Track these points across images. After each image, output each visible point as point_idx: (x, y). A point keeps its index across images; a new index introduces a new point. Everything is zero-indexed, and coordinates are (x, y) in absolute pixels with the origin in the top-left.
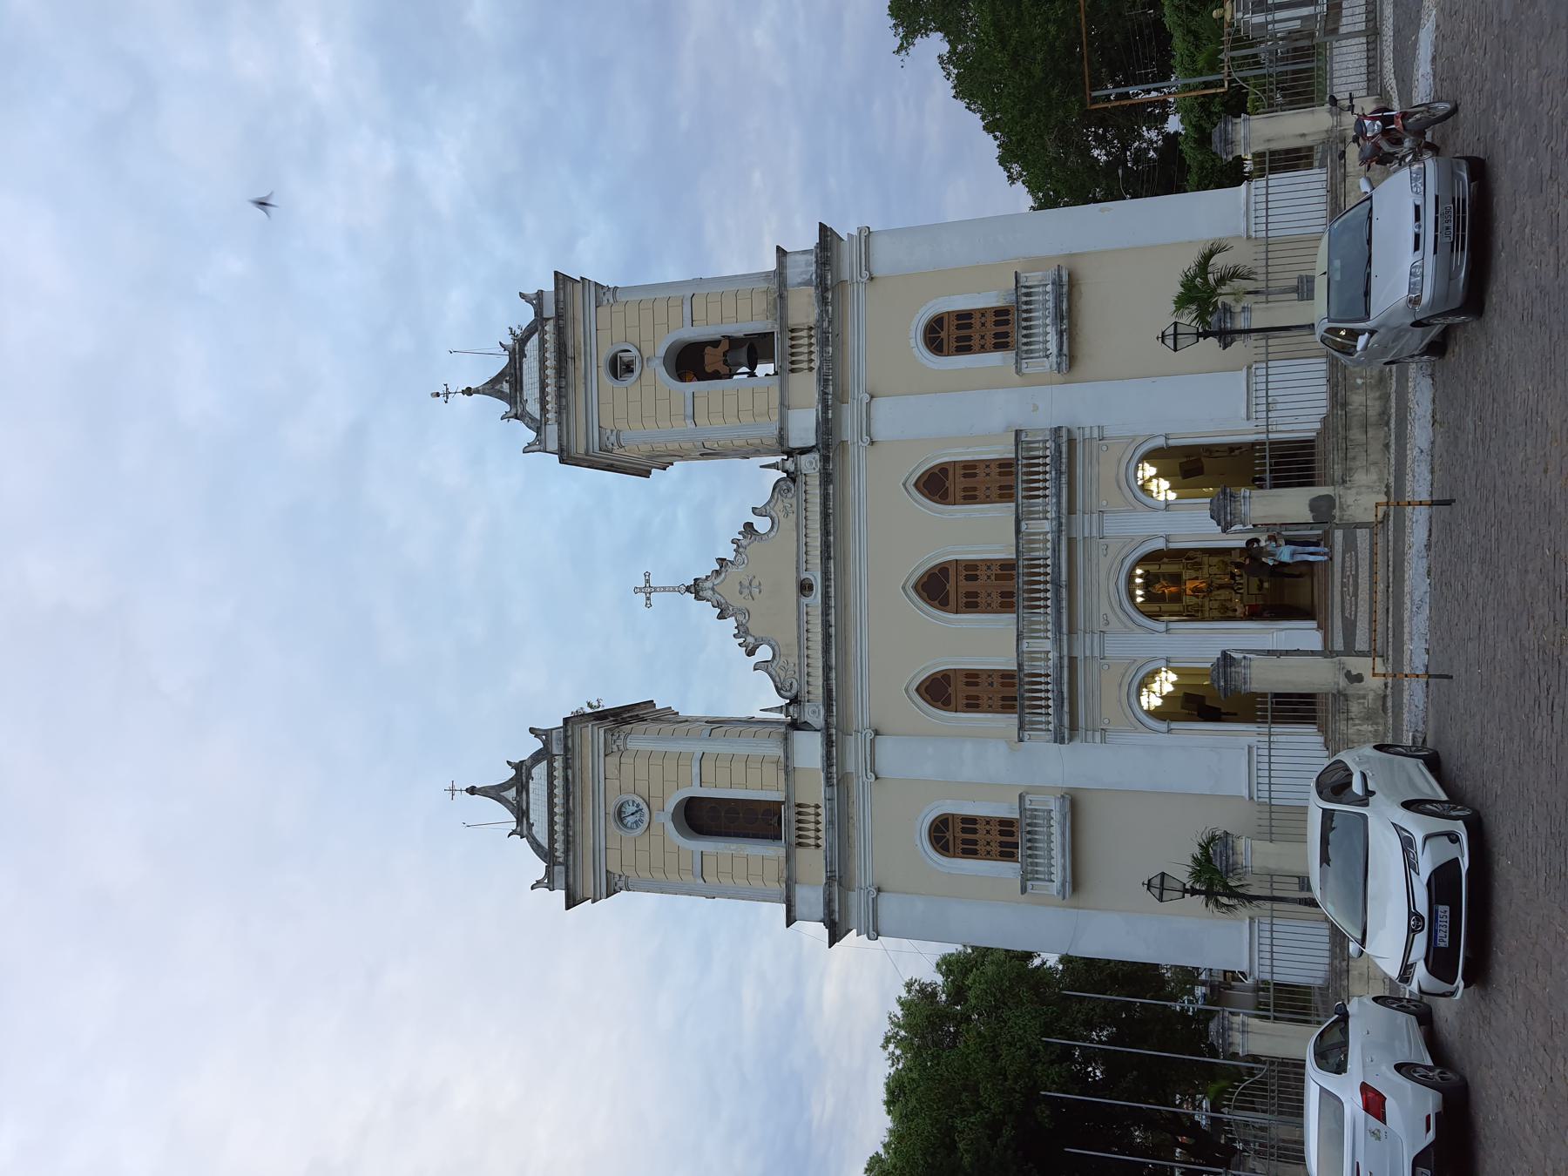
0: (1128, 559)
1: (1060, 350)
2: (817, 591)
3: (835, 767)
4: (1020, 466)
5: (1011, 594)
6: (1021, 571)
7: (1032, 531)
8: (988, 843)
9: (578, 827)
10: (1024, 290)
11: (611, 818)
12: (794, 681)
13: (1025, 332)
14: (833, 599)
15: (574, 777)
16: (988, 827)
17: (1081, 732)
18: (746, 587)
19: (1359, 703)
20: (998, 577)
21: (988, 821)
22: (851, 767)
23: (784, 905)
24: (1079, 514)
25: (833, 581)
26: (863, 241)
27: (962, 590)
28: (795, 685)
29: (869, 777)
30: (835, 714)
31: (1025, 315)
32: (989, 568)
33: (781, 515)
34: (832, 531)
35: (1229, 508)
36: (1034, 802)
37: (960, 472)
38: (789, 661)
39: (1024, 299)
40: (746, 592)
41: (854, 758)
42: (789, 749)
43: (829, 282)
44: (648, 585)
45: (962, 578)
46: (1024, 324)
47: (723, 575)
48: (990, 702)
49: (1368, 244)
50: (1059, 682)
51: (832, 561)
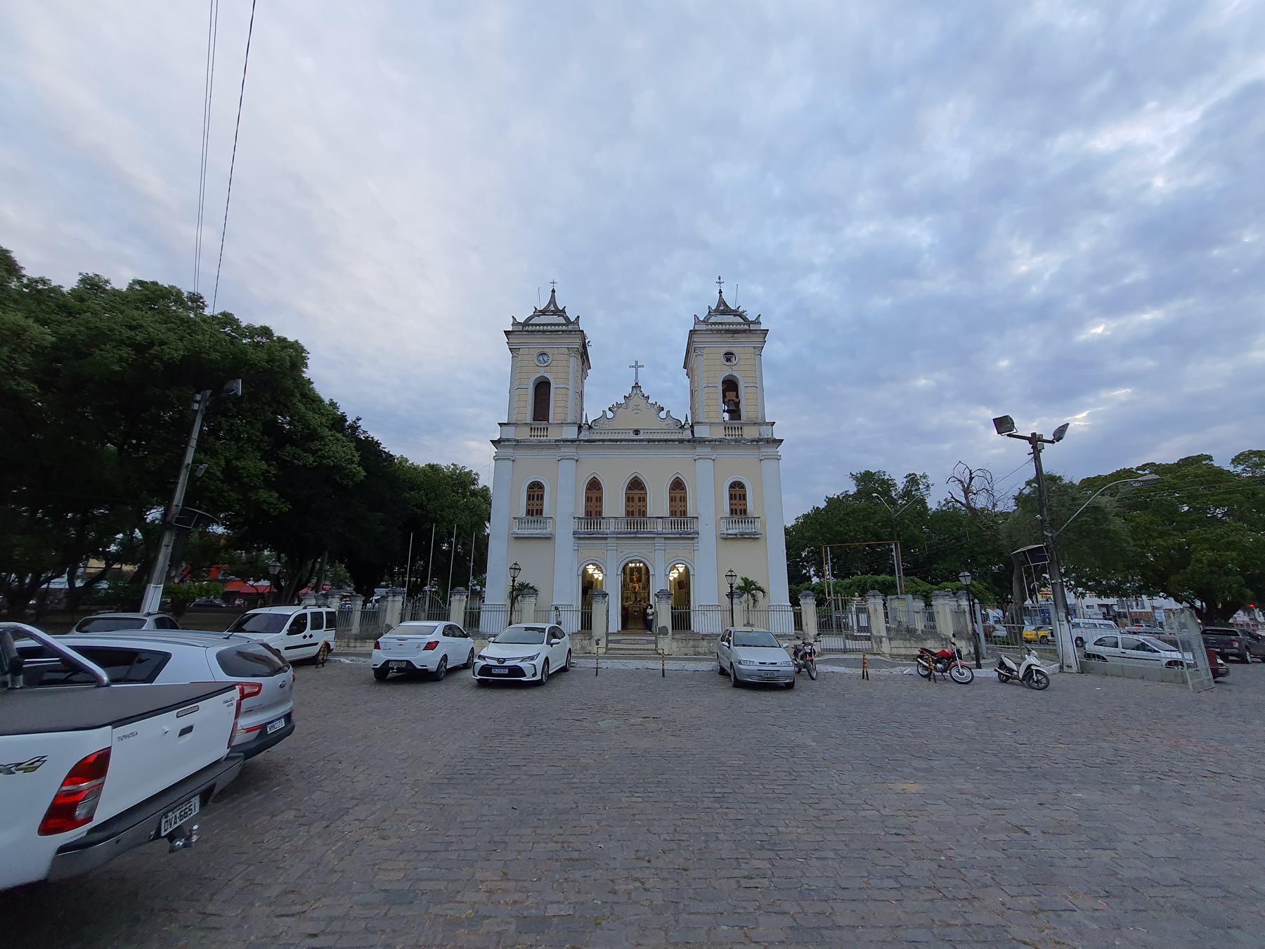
22: (563, 450)
24: (664, 541)
36: (550, 523)
40: (635, 407)
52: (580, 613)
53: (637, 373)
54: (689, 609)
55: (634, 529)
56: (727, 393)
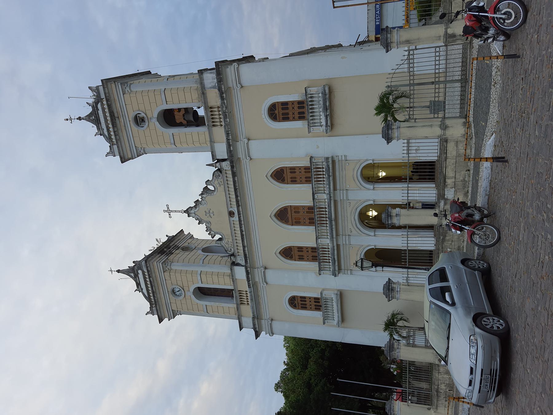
0: (359, 208)
1: (327, 124)
2: (236, 216)
3: (251, 281)
4: (313, 172)
5: (313, 219)
6: (316, 214)
7: (319, 198)
8: (311, 305)
9: (158, 296)
10: (309, 96)
11: (170, 293)
12: (232, 248)
13: (311, 114)
14: (243, 221)
15: (153, 280)
16: (310, 300)
17: (343, 271)
18: (208, 213)
19: (444, 368)
20: (307, 212)
22: (257, 280)
23: (238, 320)
24: (338, 192)
25: (242, 214)
26: (236, 70)
28: (232, 249)
30: (249, 262)
31: (310, 107)
32: (303, 209)
33: (218, 186)
34: (239, 195)
35: (391, 295)
36: (327, 294)
38: (229, 241)
39: (310, 99)
40: (208, 215)
41: (258, 276)
42: (233, 273)
43: (223, 89)
44: (168, 209)
46: (311, 111)
47: (198, 208)
48: (308, 258)
49: (448, 339)
50: (333, 254)
51: (240, 207)
52: (410, 270)
53: (176, 211)
54: (405, 250)
55: (326, 221)
56: (178, 122)
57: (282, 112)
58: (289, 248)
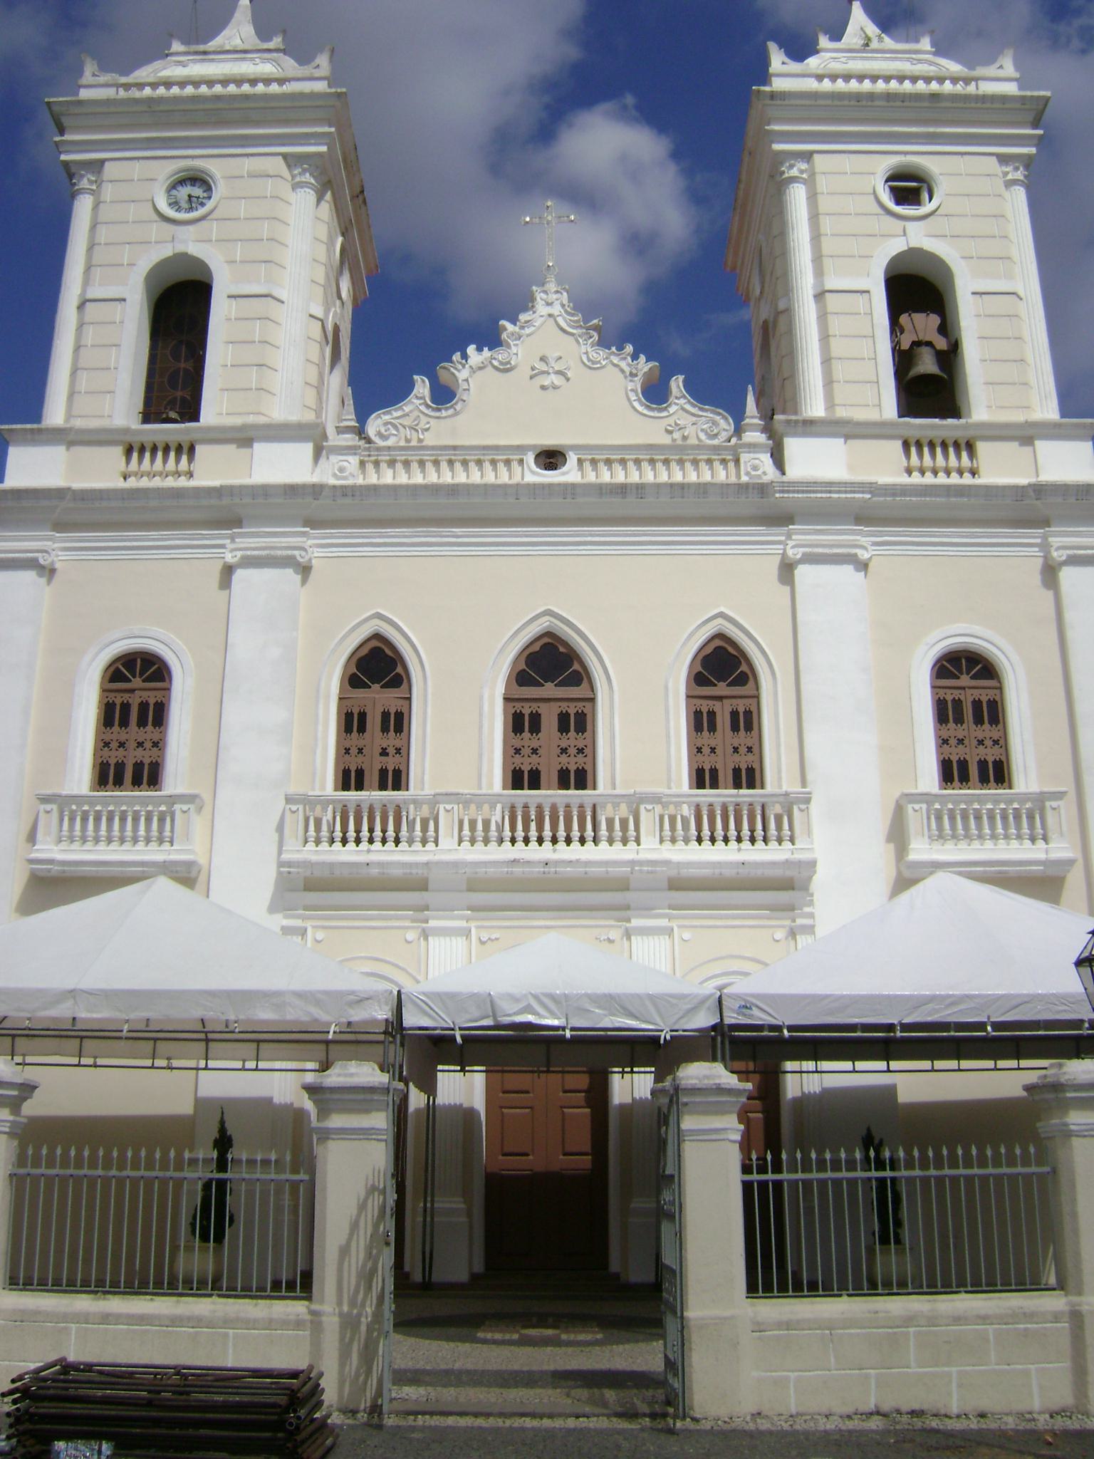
21: (159, 744)
27: (543, 709)
29: (235, 553)
37: (741, 706)
45: (564, 706)
57: (968, 698)
58: (398, 675)
